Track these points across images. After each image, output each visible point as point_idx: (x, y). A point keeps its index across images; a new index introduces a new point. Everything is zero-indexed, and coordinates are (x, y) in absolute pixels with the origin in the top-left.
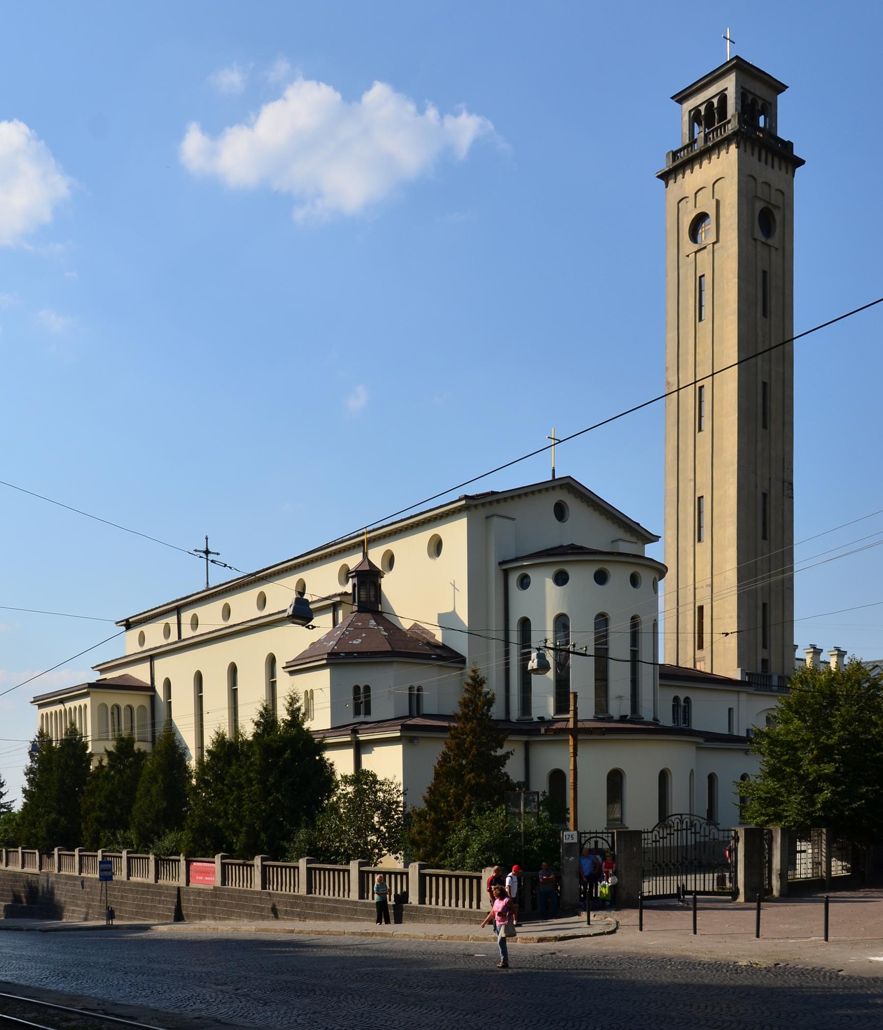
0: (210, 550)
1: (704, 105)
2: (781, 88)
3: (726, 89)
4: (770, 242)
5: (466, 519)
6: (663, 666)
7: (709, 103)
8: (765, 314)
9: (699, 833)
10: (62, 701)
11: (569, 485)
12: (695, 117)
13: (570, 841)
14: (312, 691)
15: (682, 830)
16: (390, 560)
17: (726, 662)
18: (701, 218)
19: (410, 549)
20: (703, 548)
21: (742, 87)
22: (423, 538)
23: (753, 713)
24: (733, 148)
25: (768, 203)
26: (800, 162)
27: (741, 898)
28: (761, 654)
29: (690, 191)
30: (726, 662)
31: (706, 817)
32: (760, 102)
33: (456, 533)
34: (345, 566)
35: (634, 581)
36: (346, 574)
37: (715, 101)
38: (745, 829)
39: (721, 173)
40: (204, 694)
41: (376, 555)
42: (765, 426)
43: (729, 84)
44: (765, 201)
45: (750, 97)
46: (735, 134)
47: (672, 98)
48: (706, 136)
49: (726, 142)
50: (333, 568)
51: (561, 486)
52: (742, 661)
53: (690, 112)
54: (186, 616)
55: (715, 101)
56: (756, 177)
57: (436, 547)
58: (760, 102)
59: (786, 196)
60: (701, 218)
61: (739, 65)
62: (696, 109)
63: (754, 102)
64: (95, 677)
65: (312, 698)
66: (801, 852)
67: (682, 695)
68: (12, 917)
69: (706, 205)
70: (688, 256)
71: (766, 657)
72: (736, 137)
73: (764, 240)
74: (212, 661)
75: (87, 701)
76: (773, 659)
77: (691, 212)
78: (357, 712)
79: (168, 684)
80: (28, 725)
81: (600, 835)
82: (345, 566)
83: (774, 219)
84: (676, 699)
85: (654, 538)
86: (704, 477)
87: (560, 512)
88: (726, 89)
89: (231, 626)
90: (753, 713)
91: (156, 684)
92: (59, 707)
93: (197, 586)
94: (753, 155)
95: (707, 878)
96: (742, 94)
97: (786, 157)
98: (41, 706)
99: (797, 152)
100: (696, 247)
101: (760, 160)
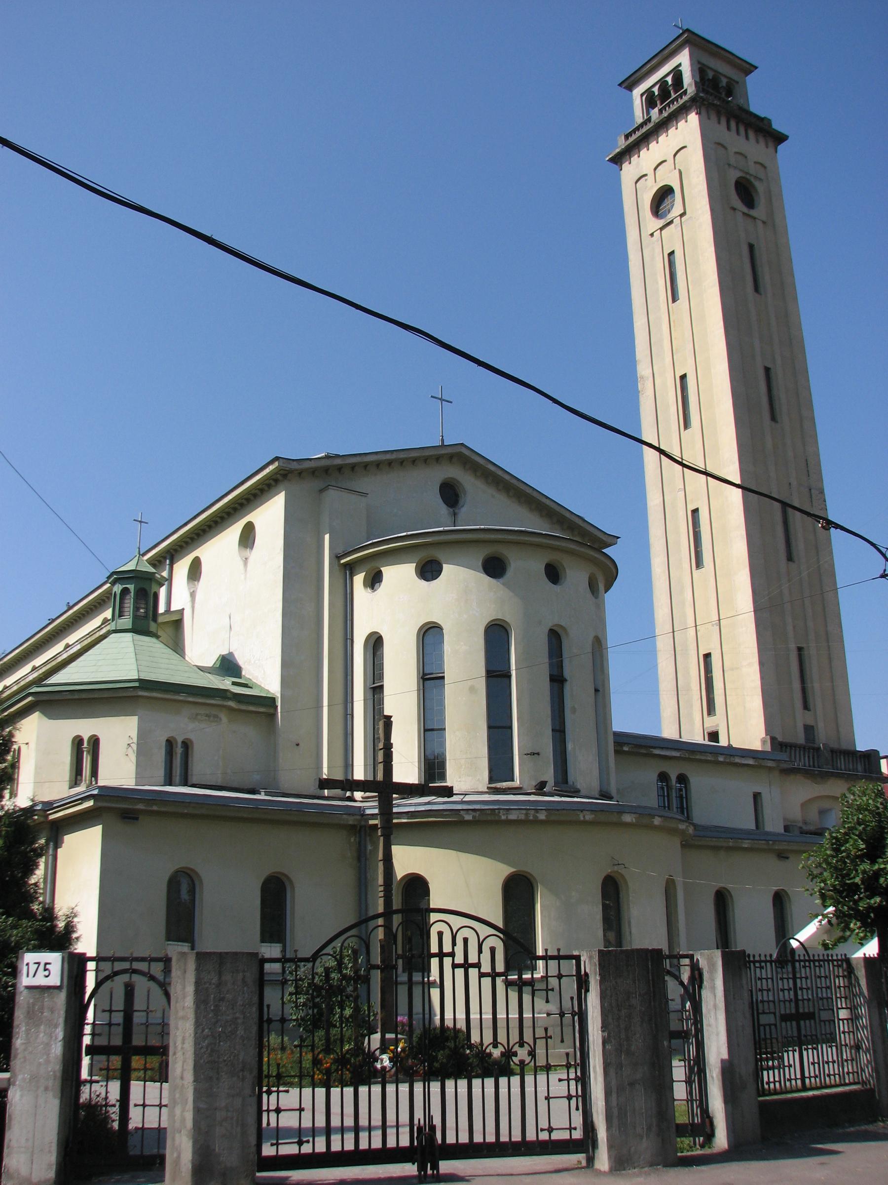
1: (657, 87)
2: (748, 68)
3: (680, 65)
4: (753, 213)
7: (662, 82)
8: (757, 289)
9: (478, 965)
13: (40, 980)
17: (746, 726)
18: (664, 195)
21: (699, 63)
22: (234, 531)
23: (790, 800)
24: (693, 118)
25: (747, 173)
27: (603, 1161)
28: (801, 718)
30: (746, 726)
31: (500, 924)
32: (724, 81)
39: (682, 150)
42: (773, 418)
43: (684, 59)
44: (741, 170)
46: (693, 100)
47: (620, 85)
49: (683, 111)
53: (642, 95)
55: (669, 79)
56: (725, 145)
57: (248, 538)
61: (691, 39)
62: (649, 92)
70: (652, 235)
71: (810, 722)
72: (695, 103)
73: (745, 210)
77: (652, 187)
81: (142, 966)
83: (756, 191)
84: (78, 742)
87: (451, 494)
88: (680, 65)
90: (790, 800)
94: (719, 123)
95: (503, 1090)
96: (701, 71)
101: (729, 128)
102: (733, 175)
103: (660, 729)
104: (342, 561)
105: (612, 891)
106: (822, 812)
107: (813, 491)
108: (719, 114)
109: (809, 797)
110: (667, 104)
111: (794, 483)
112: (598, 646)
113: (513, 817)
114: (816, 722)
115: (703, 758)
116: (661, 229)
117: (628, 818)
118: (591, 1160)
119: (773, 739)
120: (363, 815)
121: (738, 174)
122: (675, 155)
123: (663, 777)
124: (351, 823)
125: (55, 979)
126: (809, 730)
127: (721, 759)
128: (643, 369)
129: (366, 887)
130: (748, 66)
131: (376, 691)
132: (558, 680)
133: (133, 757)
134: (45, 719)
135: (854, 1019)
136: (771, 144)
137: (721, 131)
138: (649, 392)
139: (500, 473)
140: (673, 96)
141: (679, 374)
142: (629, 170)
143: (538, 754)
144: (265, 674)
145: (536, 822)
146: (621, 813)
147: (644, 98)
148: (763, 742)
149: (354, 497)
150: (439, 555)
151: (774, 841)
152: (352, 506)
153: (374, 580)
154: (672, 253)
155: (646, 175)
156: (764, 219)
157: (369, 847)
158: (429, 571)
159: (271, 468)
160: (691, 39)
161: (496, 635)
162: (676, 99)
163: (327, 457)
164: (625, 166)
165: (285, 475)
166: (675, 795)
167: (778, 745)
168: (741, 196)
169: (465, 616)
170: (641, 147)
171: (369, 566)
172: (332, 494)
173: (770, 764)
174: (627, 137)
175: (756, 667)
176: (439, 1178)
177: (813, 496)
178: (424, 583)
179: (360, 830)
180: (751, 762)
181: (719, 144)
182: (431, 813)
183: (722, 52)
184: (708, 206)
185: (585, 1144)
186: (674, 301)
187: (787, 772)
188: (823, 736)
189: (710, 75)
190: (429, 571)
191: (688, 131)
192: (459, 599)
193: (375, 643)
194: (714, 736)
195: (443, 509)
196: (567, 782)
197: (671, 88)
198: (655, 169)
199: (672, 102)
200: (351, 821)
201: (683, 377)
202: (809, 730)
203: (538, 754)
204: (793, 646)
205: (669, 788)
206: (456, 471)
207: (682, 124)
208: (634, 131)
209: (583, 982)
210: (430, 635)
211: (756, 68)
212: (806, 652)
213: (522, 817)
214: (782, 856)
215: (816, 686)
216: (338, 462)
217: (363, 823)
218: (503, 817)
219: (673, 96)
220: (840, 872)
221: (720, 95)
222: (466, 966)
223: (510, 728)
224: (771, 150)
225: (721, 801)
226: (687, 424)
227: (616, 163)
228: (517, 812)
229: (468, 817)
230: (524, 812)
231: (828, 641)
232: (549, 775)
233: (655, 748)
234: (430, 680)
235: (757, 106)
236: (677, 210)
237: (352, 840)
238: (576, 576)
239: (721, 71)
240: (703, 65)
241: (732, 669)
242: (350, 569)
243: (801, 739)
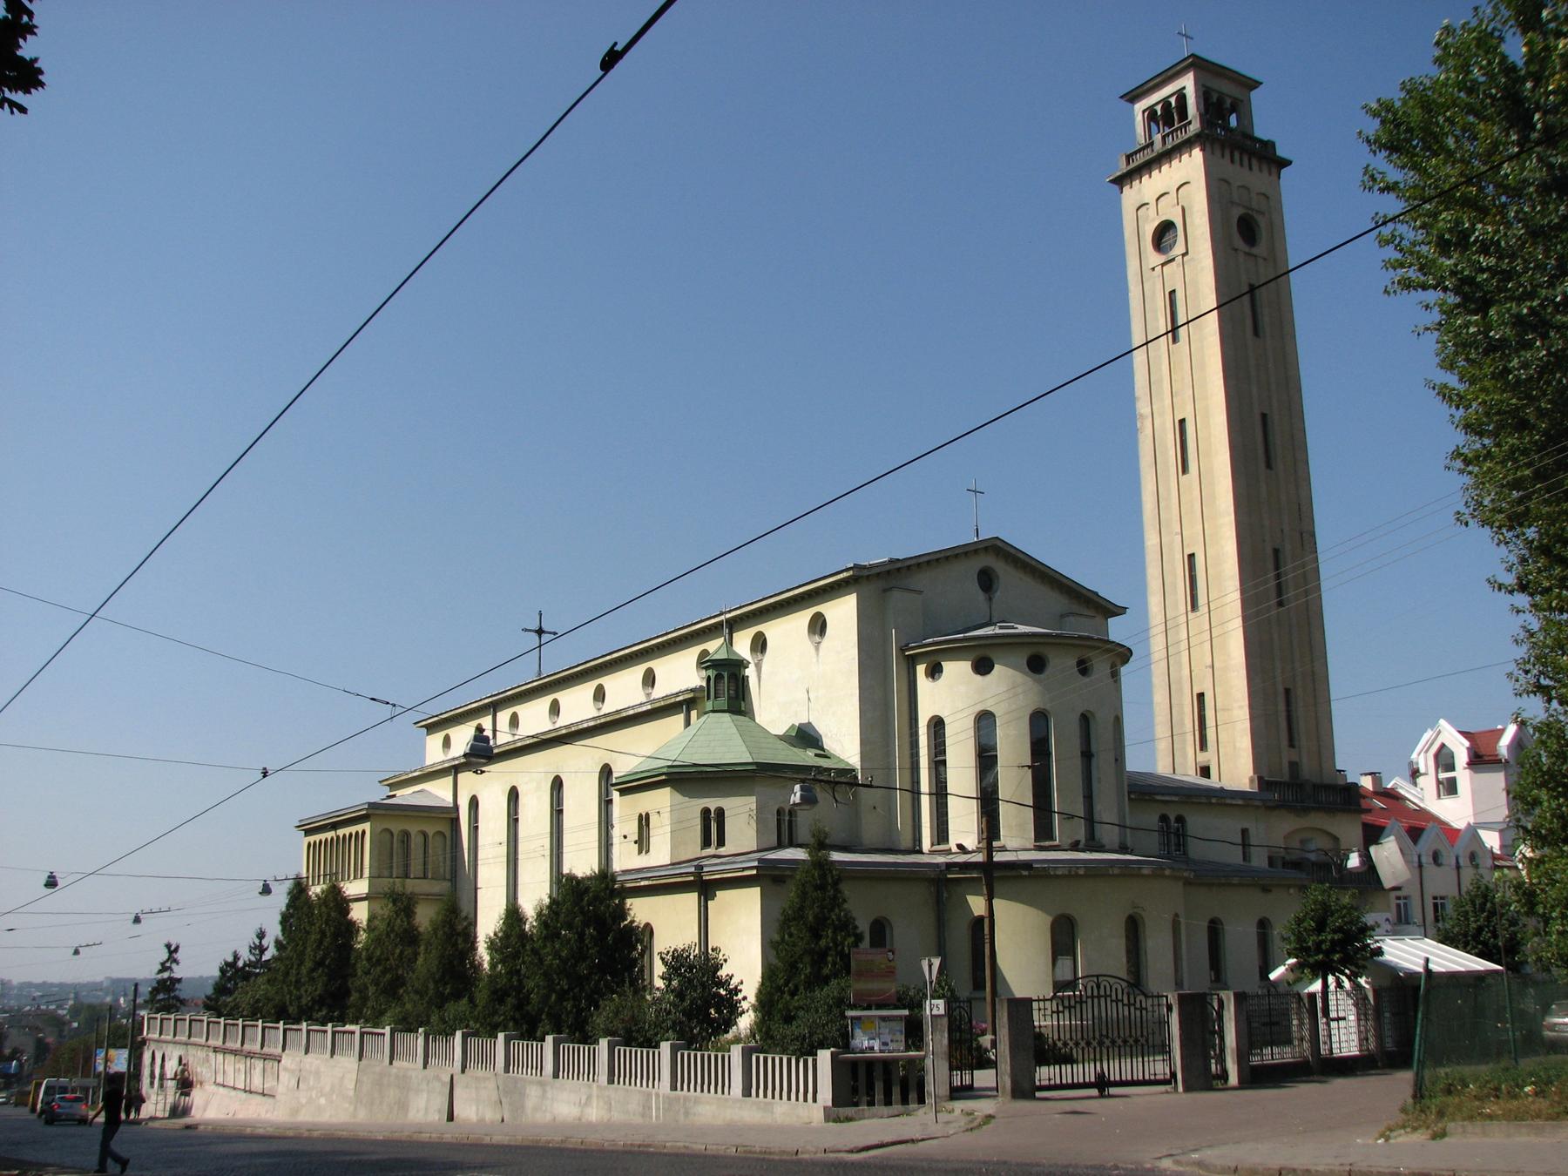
0: (545, 628)
2: (1254, 84)
4: (1255, 251)
5: (854, 596)
6: (571, 878)
7: (1165, 102)
8: (1256, 332)
10: (334, 826)
11: (997, 548)
12: (1151, 114)
14: (647, 815)
15: (1099, 997)
16: (760, 644)
17: (1236, 767)
18: (1165, 228)
19: (787, 632)
20: (1200, 619)
22: (802, 618)
23: (1277, 831)
24: (1197, 153)
26: (1285, 163)
27: (1180, 1088)
28: (1287, 755)
29: (1150, 197)
32: (1228, 102)
33: (843, 612)
34: (705, 653)
35: (1084, 668)
36: (704, 662)
37: (1173, 100)
39: (1182, 187)
40: (480, 825)
41: (742, 644)
42: (1269, 465)
43: (1188, 82)
45: (1215, 98)
48: (1164, 138)
49: (1186, 145)
50: (690, 656)
51: (986, 549)
54: (504, 717)
55: (1173, 100)
57: (818, 626)
58: (1228, 102)
59: (1271, 201)
61: (1197, 64)
63: (1220, 102)
64: (378, 794)
65: (648, 825)
66: (1338, 1019)
67: (713, 803)
68: (922, 1040)
71: (1295, 758)
74: (532, 775)
75: (367, 826)
76: (1305, 760)
78: (706, 843)
79: (474, 803)
80: (292, 858)
82: (705, 653)
84: (706, 812)
85: (1118, 611)
86: (1193, 530)
87: (987, 581)
89: (605, 715)
91: (460, 802)
92: (330, 835)
93: (524, 674)
96: (1205, 94)
97: (1268, 158)
98: (308, 832)
99: (1281, 152)
100: (1162, 259)
101: (1232, 161)
102: (1237, 212)
103: (1154, 764)
105: (1133, 928)
108: (1223, 148)
112: (1118, 721)
113: (1059, 872)
116: (1163, 265)
118: (1176, 1088)
119: (1260, 779)
123: (1164, 818)
125: (942, 1011)
126: (1294, 766)
128: (1143, 408)
131: (939, 765)
132: (1087, 755)
133: (754, 825)
134: (679, 797)
135: (1301, 1024)
136: (1274, 170)
138: (1149, 431)
142: (1133, 195)
144: (844, 744)
145: (1077, 875)
148: (1251, 780)
150: (993, 655)
152: (918, 606)
153: (935, 672)
158: (983, 667)
159: (845, 575)
161: (1039, 720)
163: (891, 561)
165: (857, 579)
166: (1174, 836)
167: (1264, 783)
172: (896, 595)
173: (1257, 803)
174: (1128, 157)
176: (1110, 1096)
178: (979, 677)
180: (1240, 802)
185: (1170, 1080)
188: (1308, 771)
189: (1215, 98)
191: (1192, 165)
192: (1004, 691)
193: (937, 724)
194: (1205, 771)
195: (981, 596)
202: (1294, 766)
204: (1281, 689)
205: (1168, 827)
206: (994, 563)
207: (1185, 157)
209: (1170, 1008)
210: (984, 720)
214: (1266, 889)
216: (899, 565)
220: (1300, 939)
221: (1225, 125)
222: (1117, 1001)
225: (1213, 839)
226: (1185, 470)
231: (1314, 681)
232: (1081, 835)
234: (986, 759)
235: (1262, 130)
236: (1179, 249)
238: (1101, 667)
243: (1286, 778)
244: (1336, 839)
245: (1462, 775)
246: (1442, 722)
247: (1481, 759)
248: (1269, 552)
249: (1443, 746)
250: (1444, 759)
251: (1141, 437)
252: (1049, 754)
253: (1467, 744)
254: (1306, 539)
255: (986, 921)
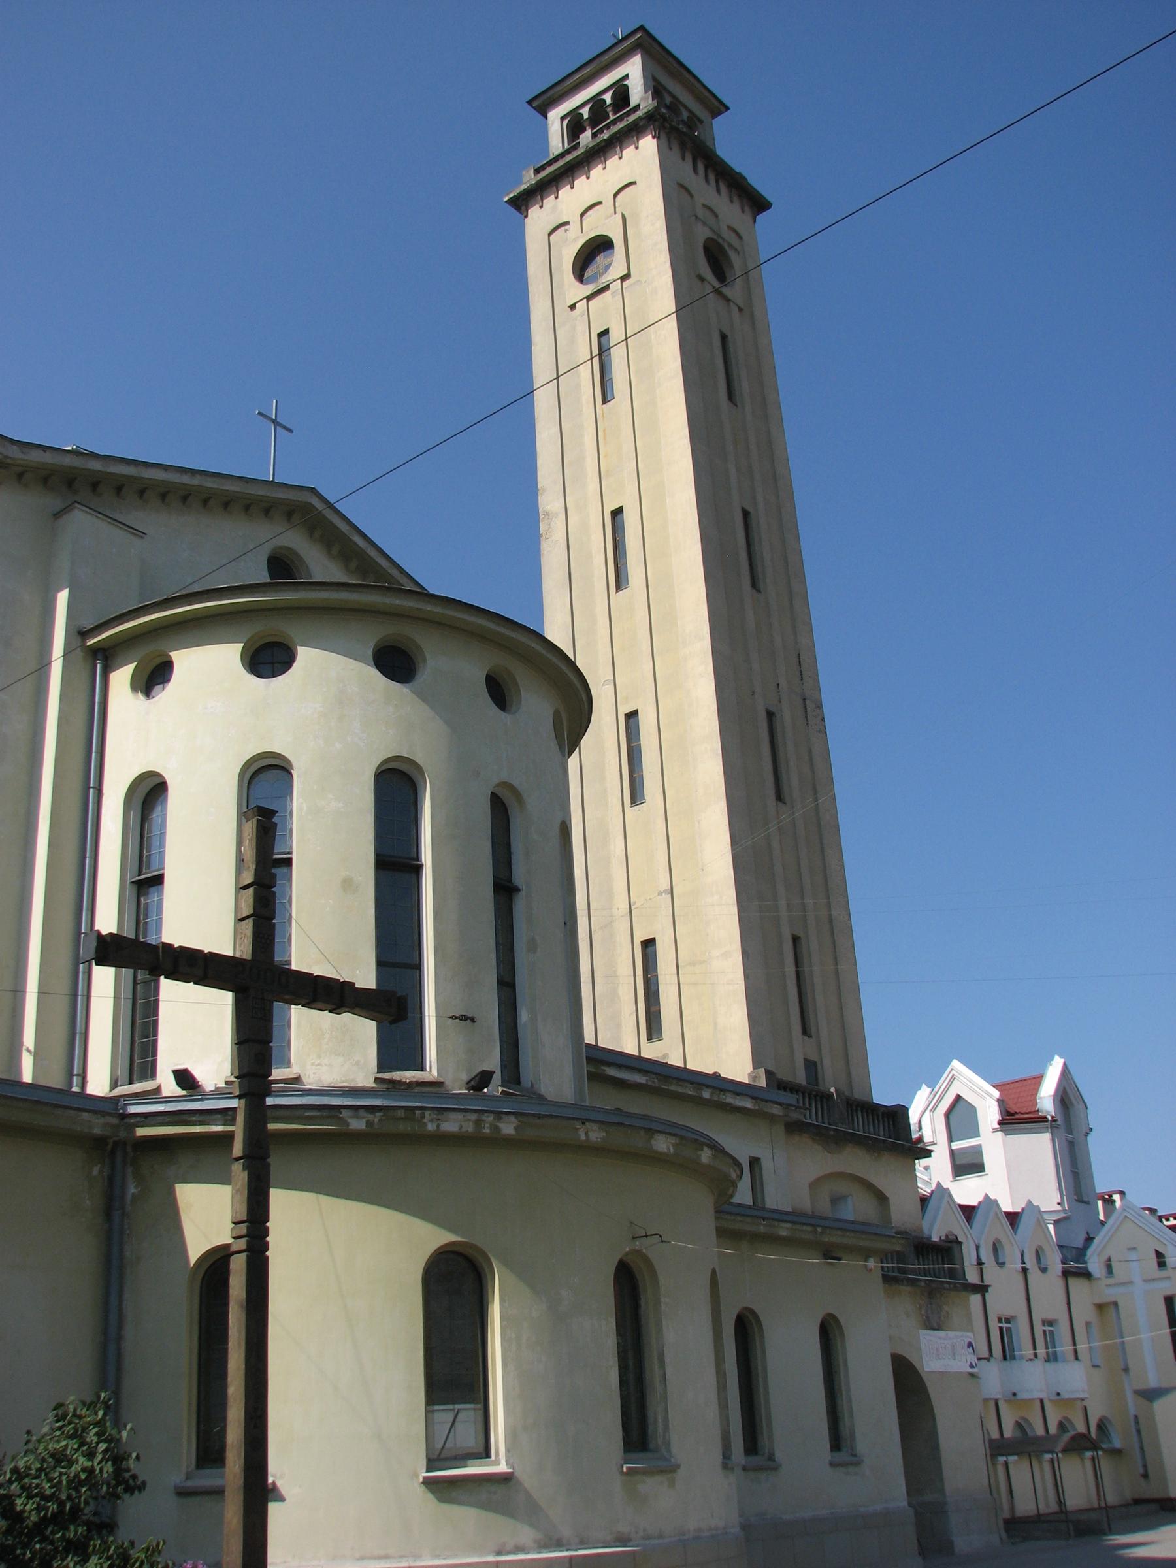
1: (587, 108)
3: (626, 77)
7: (596, 102)
11: (305, 511)
18: (598, 247)
21: (654, 79)
24: (648, 144)
28: (802, 1049)
37: (608, 98)
38: (422, 1069)
39: (631, 187)
43: (633, 70)
46: (650, 117)
47: (530, 102)
49: (634, 132)
52: (757, 1059)
53: (562, 119)
55: (608, 98)
60: (598, 247)
61: (645, 42)
69: (603, 224)
70: (573, 307)
71: (814, 1057)
73: (717, 284)
76: (827, 1062)
88: (626, 77)
94: (683, 159)
102: (702, 234)
104: (90, 642)
106: (836, 1200)
107: (808, 702)
108: (683, 146)
109: (821, 1174)
110: (604, 131)
111: (784, 685)
114: (820, 1055)
115: (679, 1090)
117: (662, 1144)
120: (125, 1116)
121: (710, 234)
122: (615, 195)
124: (97, 1131)
126: (811, 1067)
127: (706, 1094)
128: (549, 502)
129: (121, 1276)
130: (716, 103)
137: (685, 169)
139: (372, 553)
140: (612, 117)
141: (610, 506)
142: (539, 218)
143: (473, 1020)
145: (496, 1142)
146: (650, 1132)
147: (565, 123)
149: (118, 533)
151: (824, 1227)
153: (154, 677)
154: (605, 332)
155: (567, 223)
156: (741, 305)
157: (132, 1189)
158: (268, 659)
160: (645, 42)
161: (396, 787)
162: (614, 122)
164: (534, 212)
168: (711, 266)
169: (338, 746)
170: (561, 184)
171: (143, 651)
175: (737, 958)
177: (809, 709)
179: (113, 1153)
180: (748, 1104)
181: (682, 186)
182: (281, 1113)
183: (685, 73)
184: (668, 264)
186: (605, 401)
187: (794, 1128)
190: (268, 659)
191: (642, 159)
193: (149, 793)
196: (518, 1082)
197: (609, 109)
198: (582, 215)
199: (608, 127)
200: (98, 1126)
201: (617, 513)
202: (811, 1067)
203: (473, 1020)
207: (629, 152)
208: (550, 163)
210: (264, 787)
211: (727, 109)
212: (803, 942)
213: (470, 1128)
215: (821, 1001)
217: (123, 1134)
218: (431, 1127)
219: (612, 117)
221: (683, 120)
223: (418, 967)
224: (747, 217)
226: (621, 582)
227: (518, 209)
228: (460, 1116)
229: (357, 1124)
230: (474, 1117)
233: (609, 1064)
236: (617, 269)
237: (96, 1171)
239: (681, 98)
240: (662, 85)
241: (693, 964)
242: (106, 657)
243: (801, 1078)
244: (882, 1198)
245: (992, 1143)
246: (956, 1064)
247: (1016, 1118)
248: (762, 715)
249: (958, 1098)
250: (959, 1116)
251: (545, 546)
252: (418, 869)
253: (996, 1094)
254: (810, 707)
255: (238, 1266)
